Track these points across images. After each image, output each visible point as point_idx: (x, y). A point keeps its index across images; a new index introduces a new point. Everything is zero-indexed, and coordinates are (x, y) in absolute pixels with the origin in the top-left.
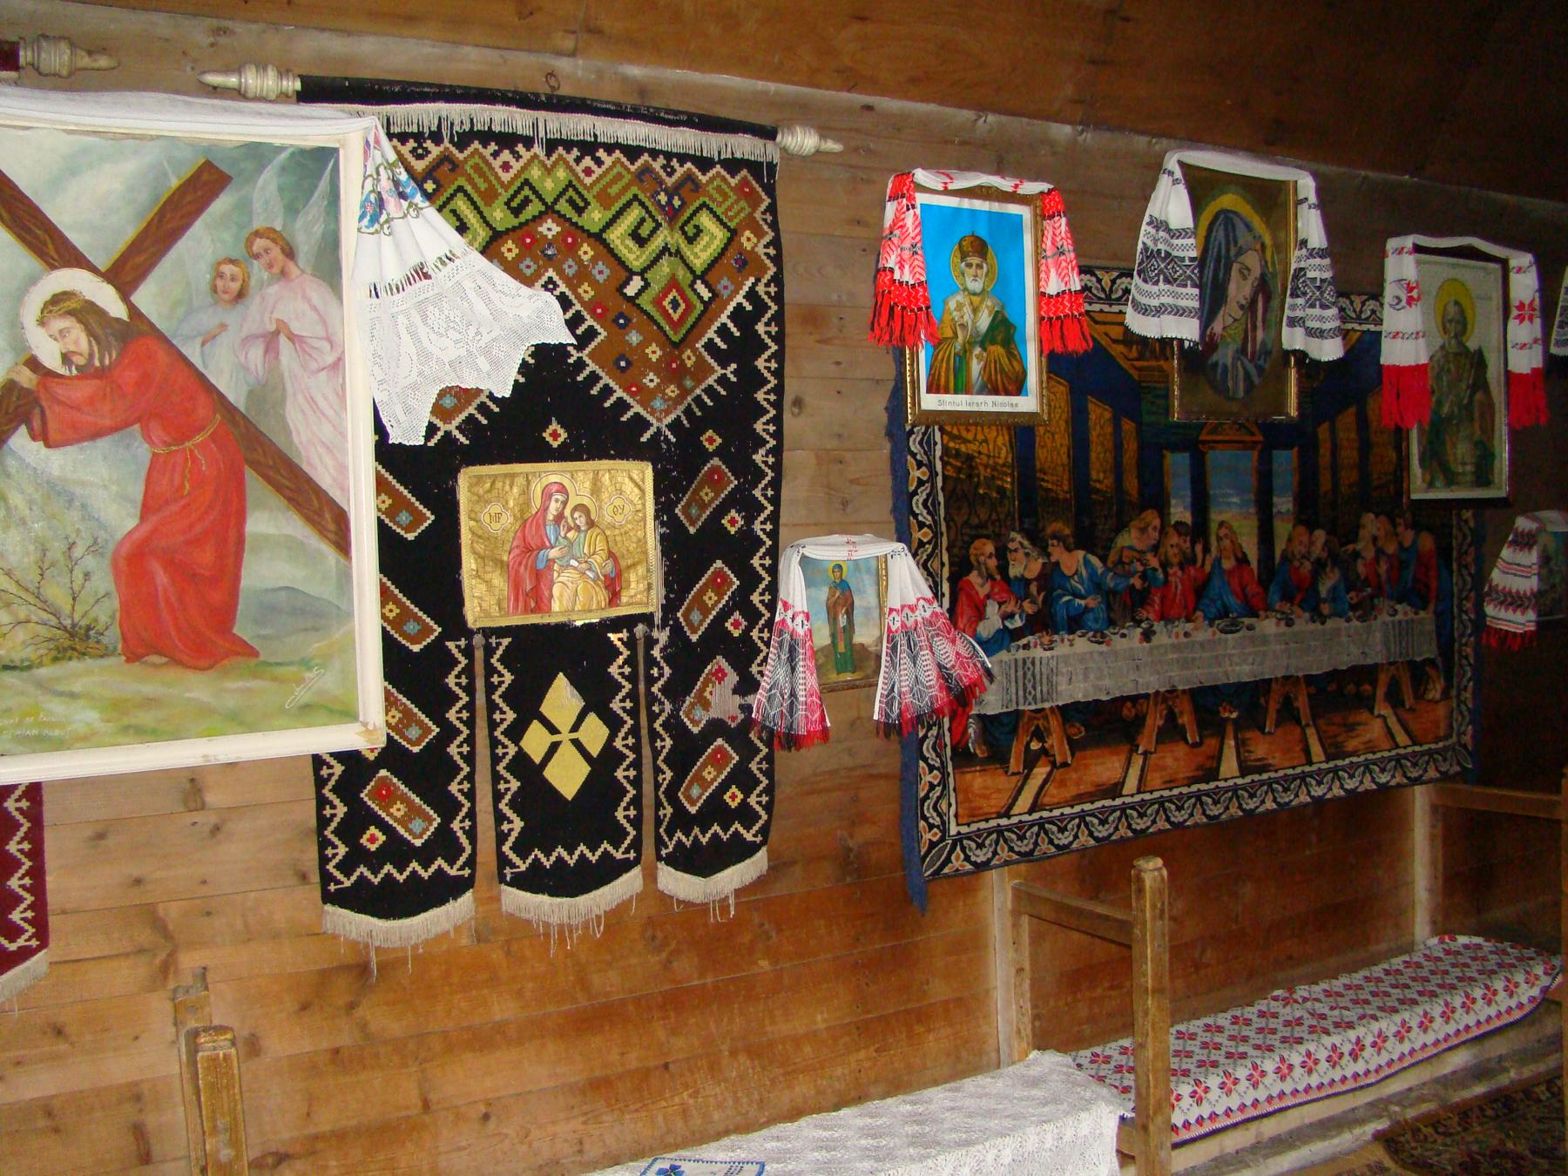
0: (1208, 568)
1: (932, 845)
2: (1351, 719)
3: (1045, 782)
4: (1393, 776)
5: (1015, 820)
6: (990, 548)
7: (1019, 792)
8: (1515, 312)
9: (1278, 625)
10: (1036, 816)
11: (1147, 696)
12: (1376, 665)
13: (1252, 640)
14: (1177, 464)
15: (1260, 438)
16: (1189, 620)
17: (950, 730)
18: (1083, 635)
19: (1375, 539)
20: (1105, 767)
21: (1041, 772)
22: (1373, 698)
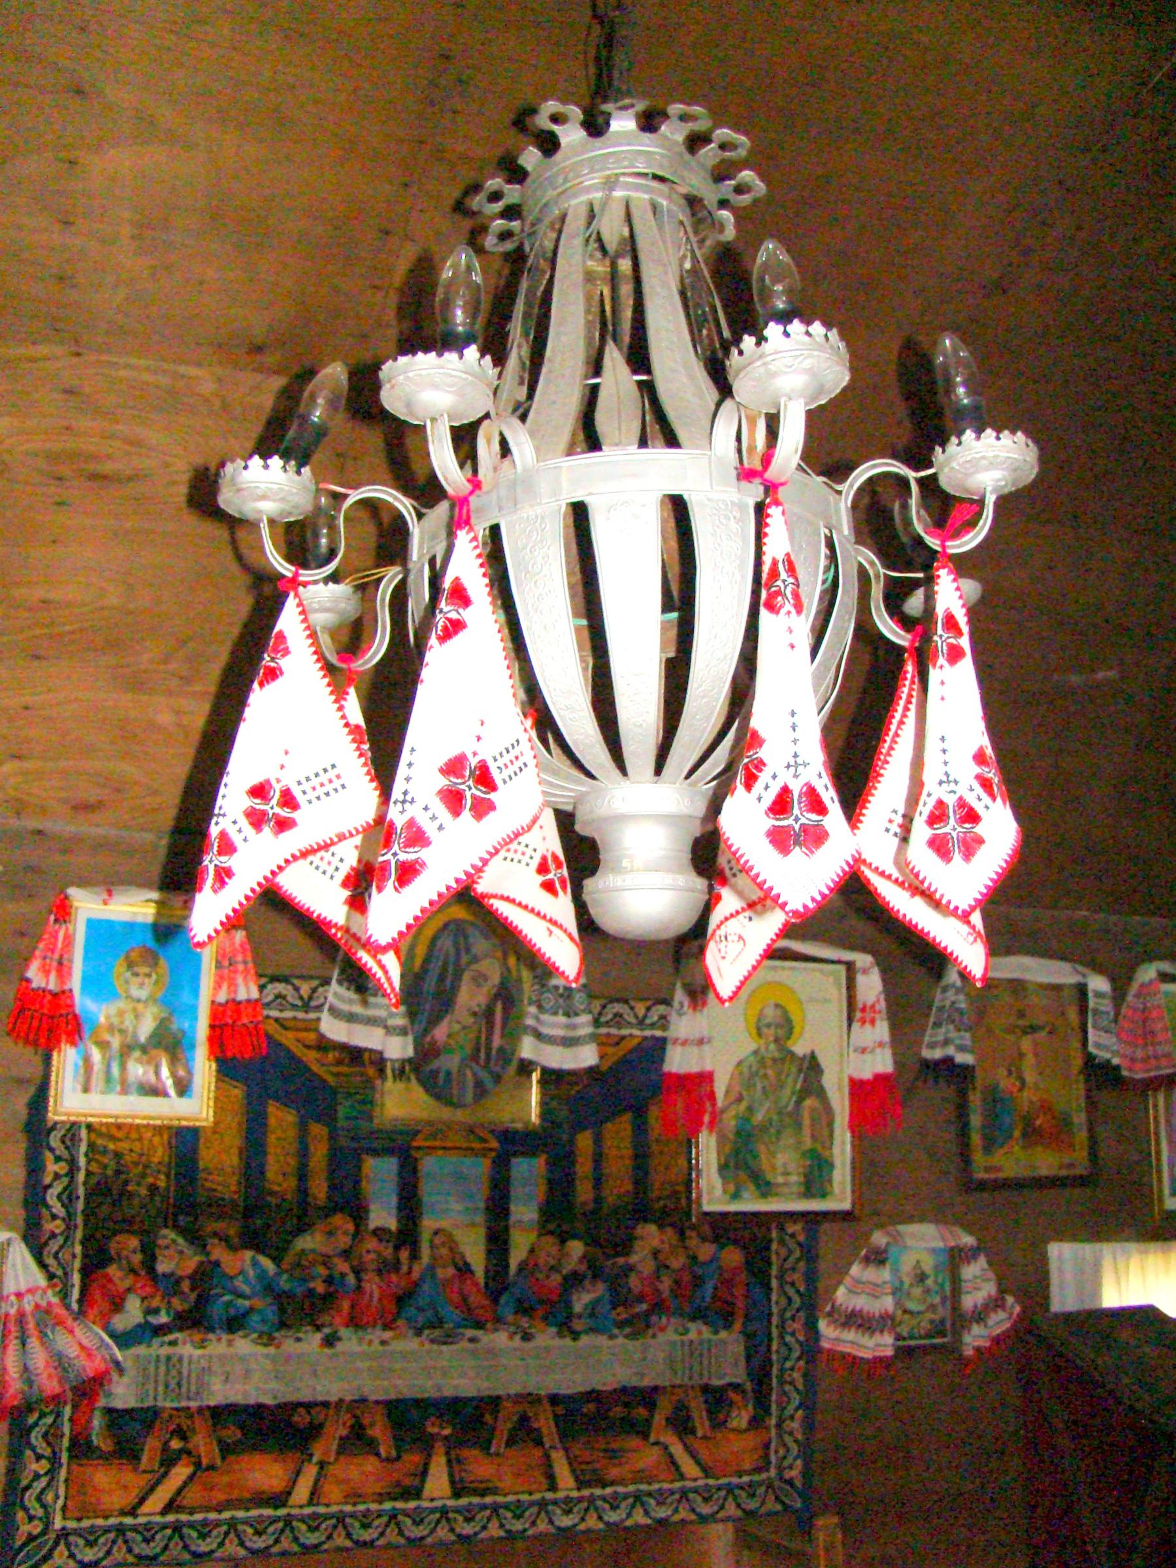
0: (415, 1275)
1: (31, 1538)
2: (615, 1446)
3: (185, 1484)
4: (676, 1511)
5: (141, 1520)
6: (134, 1242)
7: (152, 1489)
8: (858, 1015)
9: (511, 1337)
10: (171, 1518)
11: (325, 1404)
12: (656, 1389)
13: (474, 1353)
14: (380, 1174)
15: (494, 1144)
16: (387, 1326)
17: (71, 1419)
18: (246, 1336)
19: (656, 1254)
20: (265, 1472)
21: (181, 1472)
22: (648, 1422)
